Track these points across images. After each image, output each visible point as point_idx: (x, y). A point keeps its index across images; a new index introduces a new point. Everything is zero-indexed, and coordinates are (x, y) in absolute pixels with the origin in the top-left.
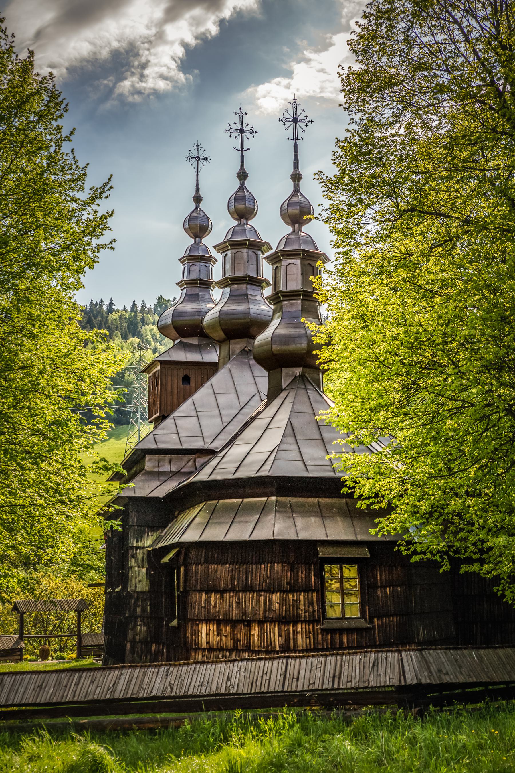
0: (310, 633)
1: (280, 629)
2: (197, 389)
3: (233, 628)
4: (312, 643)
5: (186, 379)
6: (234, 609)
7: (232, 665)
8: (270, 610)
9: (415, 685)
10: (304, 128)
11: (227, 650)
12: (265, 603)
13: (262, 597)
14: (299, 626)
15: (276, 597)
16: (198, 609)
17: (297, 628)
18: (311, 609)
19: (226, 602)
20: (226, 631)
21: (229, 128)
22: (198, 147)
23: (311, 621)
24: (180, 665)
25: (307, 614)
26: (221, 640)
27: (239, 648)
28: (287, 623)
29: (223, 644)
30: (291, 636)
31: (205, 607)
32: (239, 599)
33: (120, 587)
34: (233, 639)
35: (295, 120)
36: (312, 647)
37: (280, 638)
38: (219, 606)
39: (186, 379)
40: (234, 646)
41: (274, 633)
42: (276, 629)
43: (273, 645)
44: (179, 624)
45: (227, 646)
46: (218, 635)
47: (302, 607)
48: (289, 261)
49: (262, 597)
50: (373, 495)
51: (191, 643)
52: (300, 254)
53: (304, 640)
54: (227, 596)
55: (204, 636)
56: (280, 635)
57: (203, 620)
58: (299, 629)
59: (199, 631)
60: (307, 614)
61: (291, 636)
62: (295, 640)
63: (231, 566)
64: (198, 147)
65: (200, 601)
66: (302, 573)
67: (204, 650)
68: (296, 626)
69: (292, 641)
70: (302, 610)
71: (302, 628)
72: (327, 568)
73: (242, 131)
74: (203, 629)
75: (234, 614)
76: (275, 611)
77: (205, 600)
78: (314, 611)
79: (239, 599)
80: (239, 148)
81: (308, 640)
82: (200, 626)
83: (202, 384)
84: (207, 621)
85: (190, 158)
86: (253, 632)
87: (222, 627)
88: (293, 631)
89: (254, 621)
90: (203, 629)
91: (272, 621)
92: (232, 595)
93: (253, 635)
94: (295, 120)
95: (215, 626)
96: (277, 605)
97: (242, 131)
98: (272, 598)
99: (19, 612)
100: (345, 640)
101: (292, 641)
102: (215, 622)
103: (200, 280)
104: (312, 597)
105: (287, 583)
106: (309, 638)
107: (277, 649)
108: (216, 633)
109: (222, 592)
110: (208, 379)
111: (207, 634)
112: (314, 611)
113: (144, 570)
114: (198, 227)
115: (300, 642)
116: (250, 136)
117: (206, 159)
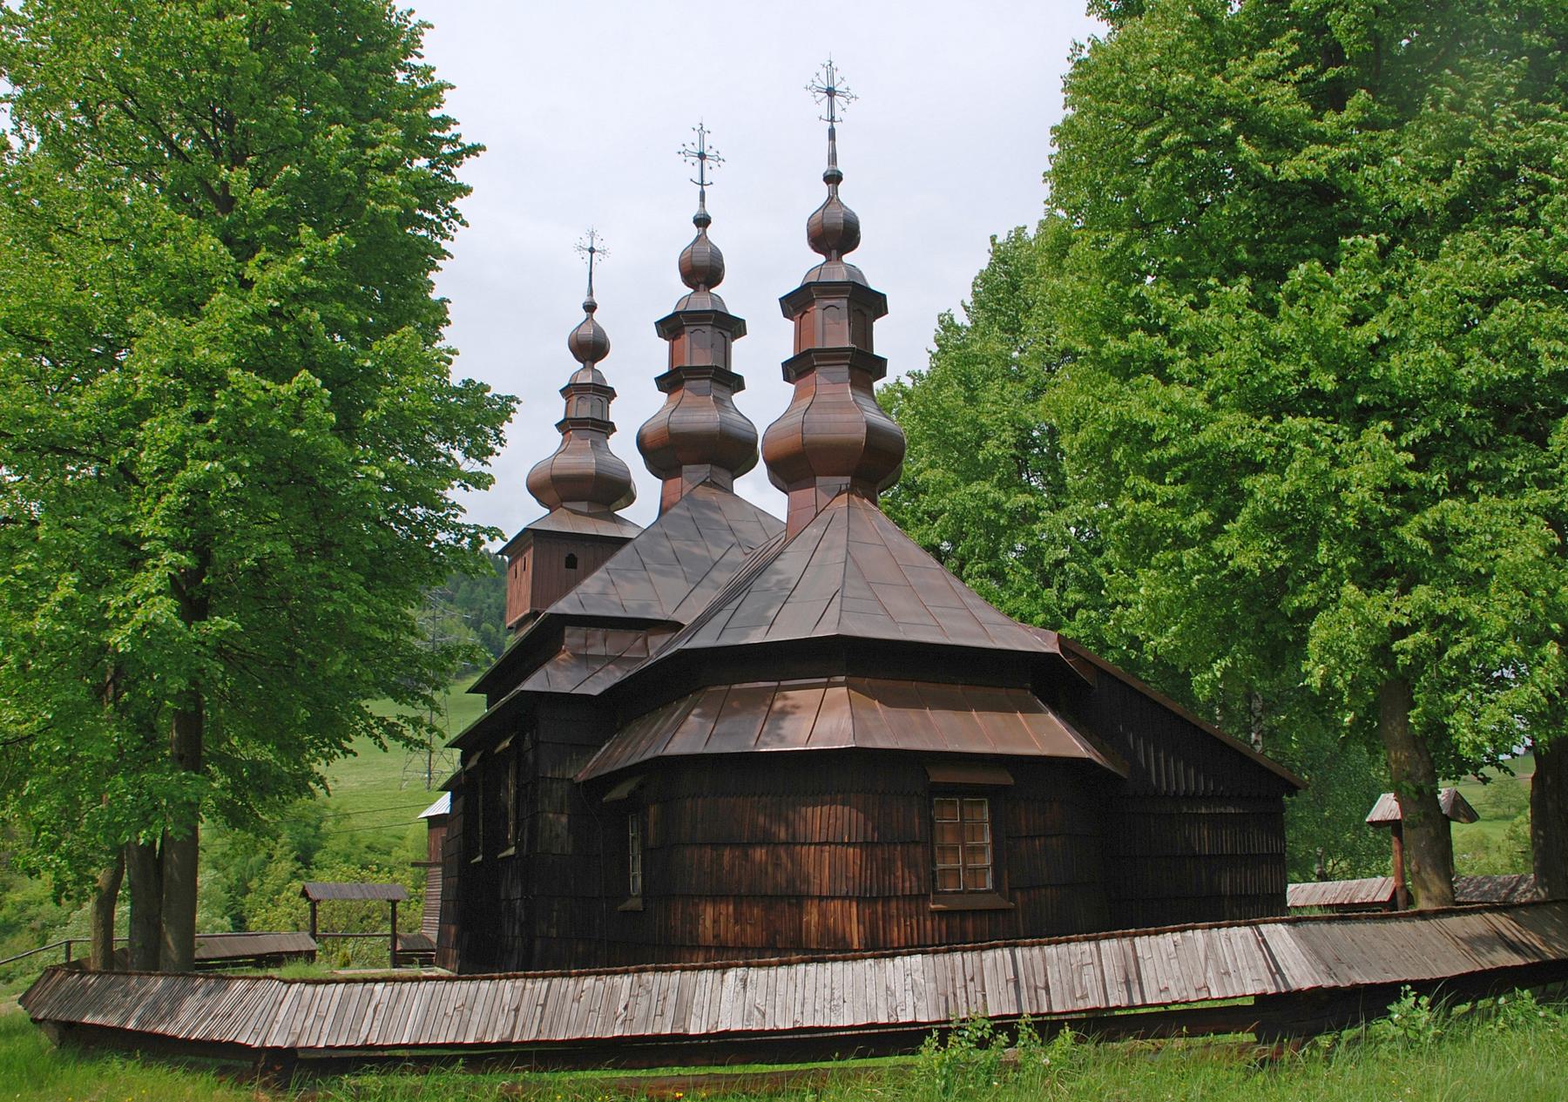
2: (586, 574)
5: (571, 562)
7: (546, 984)
14: (893, 904)
22: (592, 234)
24: (770, 965)
26: (743, 930)
35: (831, 92)
39: (571, 562)
42: (854, 910)
46: (736, 922)
55: (708, 923)
64: (592, 234)
67: (708, 948)
72: (200, 953)
73: (702, 156)
83: (595, 568)
84: (716, 897)
87: (745, 908)
88: (884, 914)
89: (812, 897)
94: (831, 92)
97: (702, 156)
99: (309, 899)
110: (603, 561)
111: (715, 921)
113: (564, 819)
114: (590, 348)
116: (714, 164)
117: (603, 252)
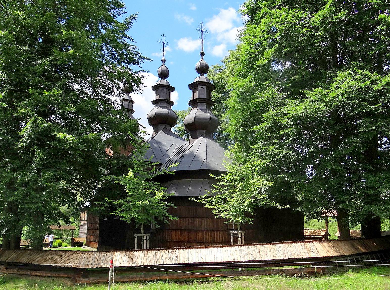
9: (380, 227)
10: (206, 35)
28: (214, 231)
29: (183, 239)
31: (175, 224)
32: (191, 221)
33: (110, 213)
42: (210, 234)
45: (185, 240)
47: (219, 225)
48: (201, 87)
50: (31, 90)
52: (206, 84)
54: (186, 219)
62: (217, 239)
64: (164, 36)
74: (174, 233)
75: (190, 227)
76: (209, 226)
79: (191, 221)
91: (207, 230)
93: (198, 236)
95: (180, 232)
115: (219, 239)
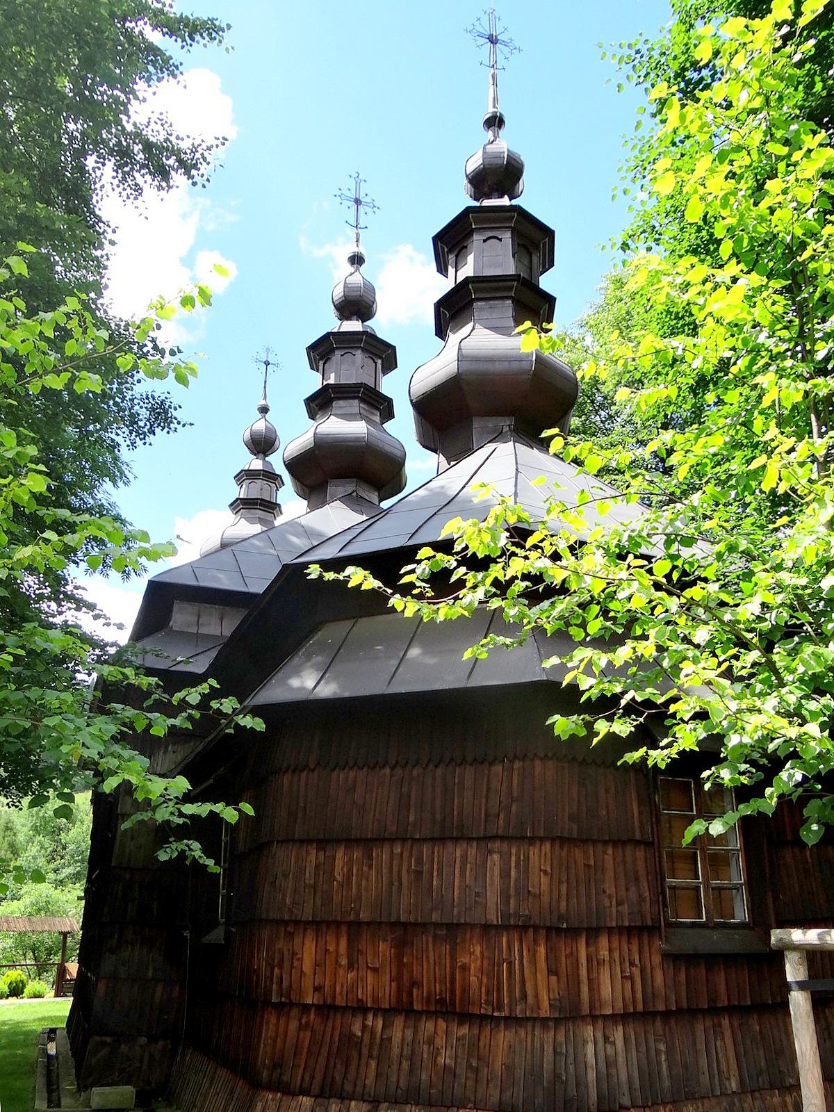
0: (632, 964)
1: (551, 950)
3: (401, 945)
4: (639, 995)
6: (405, 891)
8: (524, 891)
11: (376, 1011)
12: (505, 874)
13: (496, 857)
15: (539, 857)
16: (295, 891)
17: (597, 951)
18: (633, 895)
19: (380, 872)
20: (376, 954)
21: (339, 193)
23: (639, 931)
25: (625, 909)
27: (417, 1007)
29: (365, 993)
30: (583, 972)
31: (315, 886)
34: (398, 978)
36: (640, 1008)
37: (553, 979)
38: (359, 885)
40: (399, 1000)
41: (533, 962)
43: (530, 1000)
44: (228, 936)
46: (351, 966)
47: (610, 888)
49: (496, 857)
51: (268, 992)
53: (619, 986)
54: (382, 854)
56: (551, 971)
57: (307, 922)
58: (604, 953)
59: (294, 954)
60: (625, 909)
61: (583, 972)
63: (399, 771)
65: (301, 871)
66: (607, 791)
68: (596, 943)
69: (585, 989)
70: (610, 897)
71: (610, 951)
74: (308, 950)
77: (317, 866)
78: (641, 898)
79: (420, 861)
80: (353, 222)
81: (628, 985)
82: (297, 940)
84: (318, 926)
85: (257, 361)
86: (463, 959)
88: (589, 959)
90: (308, 950)
92: (398, 850)
93: (465, 968)
96: (545, 880)
98: (527, 858)
100: (722, 988)
101: (585, 989)
102: (344, 929)
103: (261, 500)
104: (634, 861)
105: (571, 818)
106: (631, 978)
107: (545, 1012)
108: (344, 961)
109: (368, 843)
112: (641, 898)
115: (606, 991)
